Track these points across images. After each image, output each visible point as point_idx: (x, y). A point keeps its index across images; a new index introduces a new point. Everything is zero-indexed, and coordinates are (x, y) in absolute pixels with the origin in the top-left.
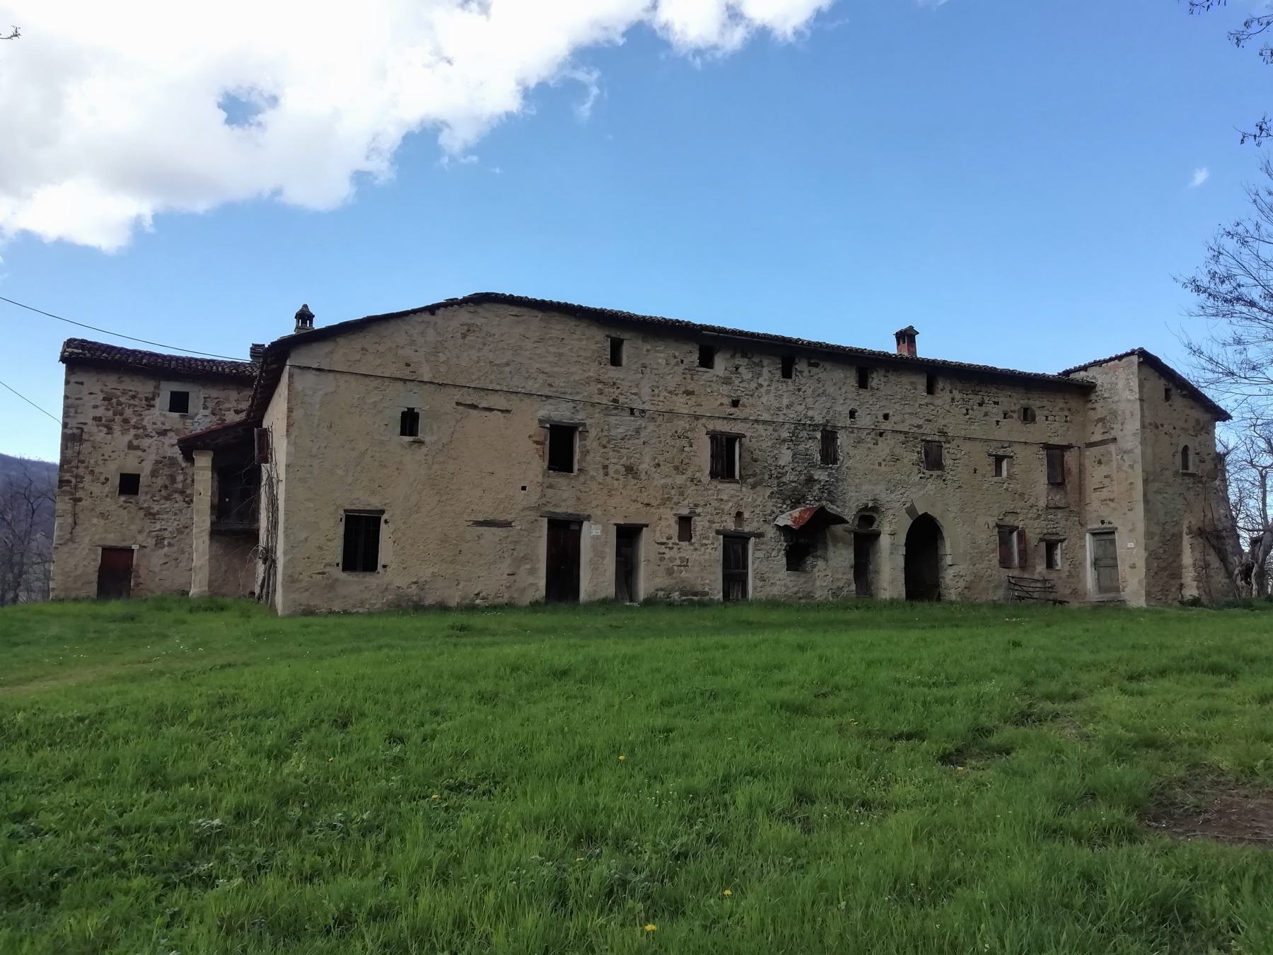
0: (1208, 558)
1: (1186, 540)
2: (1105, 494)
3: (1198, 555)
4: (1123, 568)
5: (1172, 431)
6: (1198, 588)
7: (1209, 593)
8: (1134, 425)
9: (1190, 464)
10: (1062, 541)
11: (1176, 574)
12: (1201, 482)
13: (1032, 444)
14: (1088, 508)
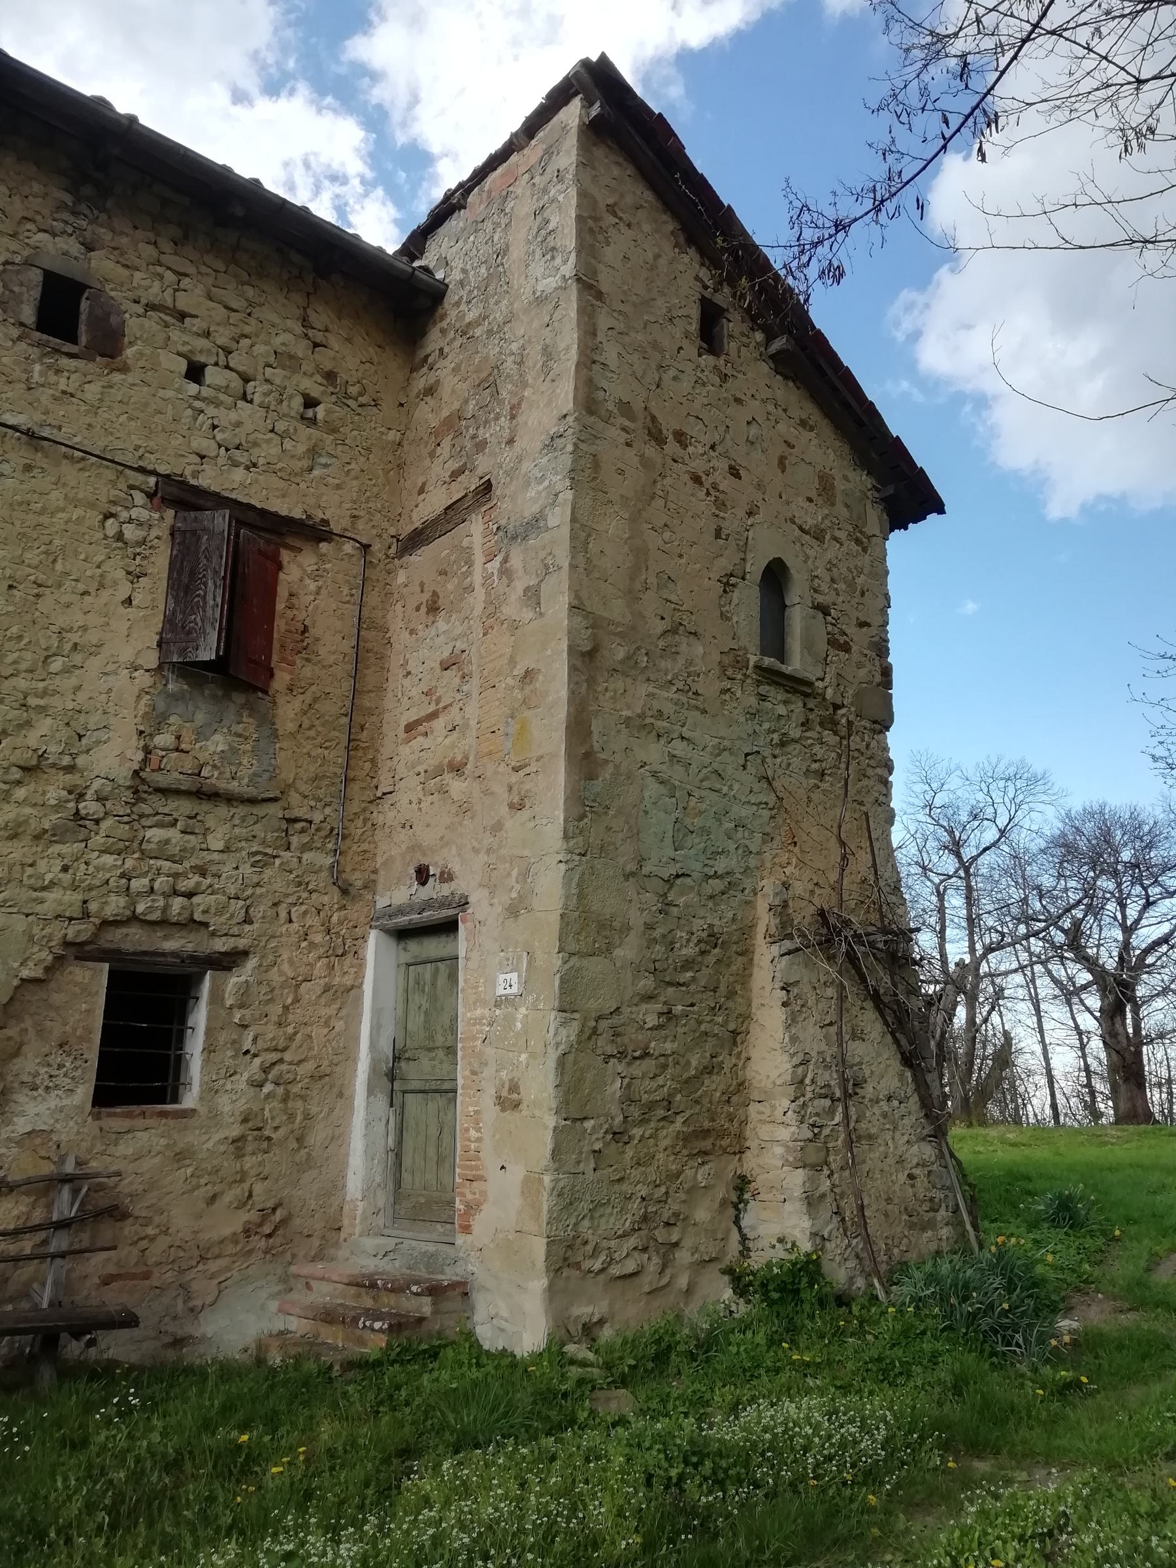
0: (857, 1050)
1: (768, 965)
2: (438, 744)
3: (814, 1039)
4: (475, 1105)
5: (726, 483)
6: (812, 1202)
7: (856, 1224)
8: (550, 402)
9: (795, 645)
10: (228, 961)
11: (717, 1136)
12: (830, 723)
13: (83, 455)
14: (387, 815)
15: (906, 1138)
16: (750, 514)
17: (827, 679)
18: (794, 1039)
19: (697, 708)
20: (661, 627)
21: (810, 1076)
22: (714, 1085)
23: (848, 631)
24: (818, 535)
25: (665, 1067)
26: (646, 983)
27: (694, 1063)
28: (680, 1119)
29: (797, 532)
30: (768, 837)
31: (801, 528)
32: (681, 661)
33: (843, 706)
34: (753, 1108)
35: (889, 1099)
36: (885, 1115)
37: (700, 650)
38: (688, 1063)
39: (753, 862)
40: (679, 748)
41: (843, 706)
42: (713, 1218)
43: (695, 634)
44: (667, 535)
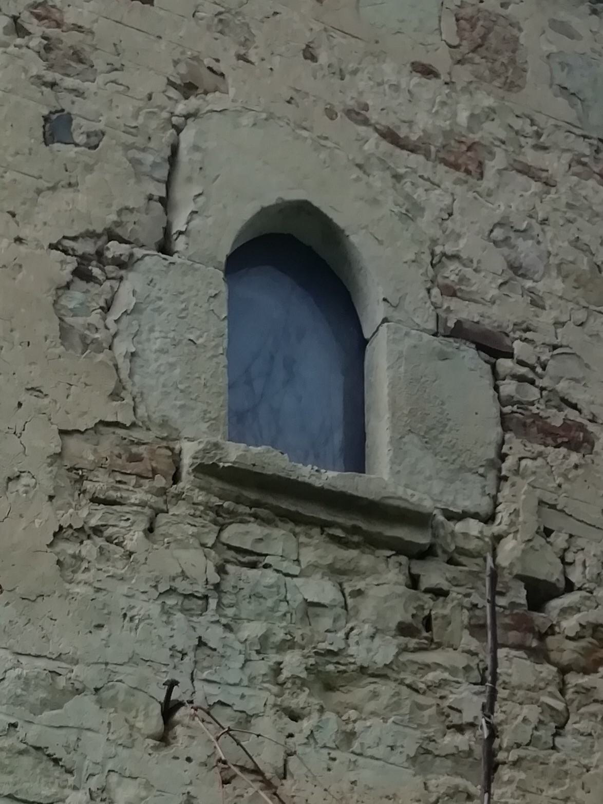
16: (188, 89)
17: (503, 515)
24: (463, 157)
29: (373, 144)
31: (390, 136)
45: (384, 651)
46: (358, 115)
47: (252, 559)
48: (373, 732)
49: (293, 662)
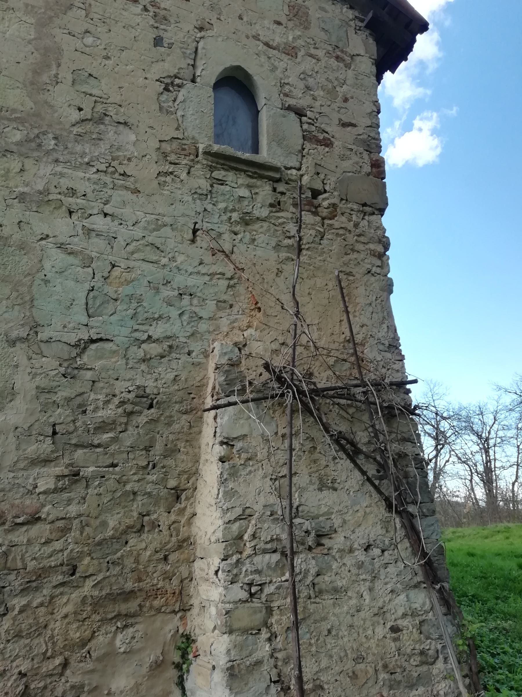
3: (258, 490)
15: (389, 587)
16: (201, 29)
17: (304, 168)
18: (230, 494)
19: (126, 188)
20: (76, 116)
21: (250, 531)
22: (144, 545)
23: (328, 129)
24: (291, 51)
25: (65, 531)
26: (46, 446)
27: (112, 523)
28: (90, 583)
29: (261, 47)
30: (223, 305)
31: (267, 44)
32: (103, 147)
33: (325, 191)
34: (198, 564)
35: (368, 548)
36: (360, 565)
37: (133, 137)
38: (104, 524)
39: (203, 327)
40: (99, 223)
41: (325, 191)
42: (137, 685)
43: (125, 124)
44: (89, 40)
45: (265, 212)
46: (256, 37)
47: (222, 182)
48: (261, 239)
49: (235, 216)
